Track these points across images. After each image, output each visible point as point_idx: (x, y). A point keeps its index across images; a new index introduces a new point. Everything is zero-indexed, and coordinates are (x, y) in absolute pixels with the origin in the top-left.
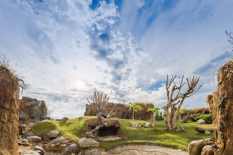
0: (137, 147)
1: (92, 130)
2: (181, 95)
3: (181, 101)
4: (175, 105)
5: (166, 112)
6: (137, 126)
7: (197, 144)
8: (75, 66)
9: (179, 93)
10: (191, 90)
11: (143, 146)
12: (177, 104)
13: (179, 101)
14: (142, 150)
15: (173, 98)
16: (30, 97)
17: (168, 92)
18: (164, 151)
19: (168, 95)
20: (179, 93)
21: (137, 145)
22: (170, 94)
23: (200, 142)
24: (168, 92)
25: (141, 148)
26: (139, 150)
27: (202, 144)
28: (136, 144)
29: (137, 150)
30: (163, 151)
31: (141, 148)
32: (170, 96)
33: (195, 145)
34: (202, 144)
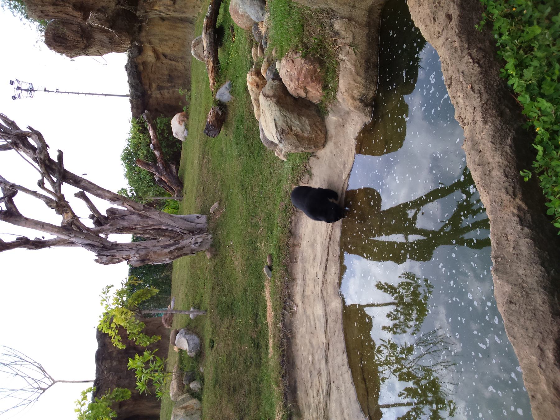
0: (312, 393)
1: (328, 161)
2: (48, 185)
3: (77, 190)
4: (99, 220)
5: (125, 254)
6: (195, 401)
7: (278, 113)
8: (312, 335)
9: (34, 193)
10: (30, 140)
11: (298, 363)
12: (92, 207)
13: (81, 195)
14: (323, 366)
15: (57, 220)
16: (298, 336)
17: (23, 242)
18: (319, 255)
19: (39, 244)
20: (34, 193)
21: (301, 394)
22: (33, 234)
23: (268, 103)
24: (23, 242)
25: (315, 373)
26: (329, 384)
27: (274, 96)
28: (295, 400)
29: (328, 393)
30: (318, 260)
31: (315, 373)
32: (48, 236)
33: (280, 123)
34: (274, 96)
